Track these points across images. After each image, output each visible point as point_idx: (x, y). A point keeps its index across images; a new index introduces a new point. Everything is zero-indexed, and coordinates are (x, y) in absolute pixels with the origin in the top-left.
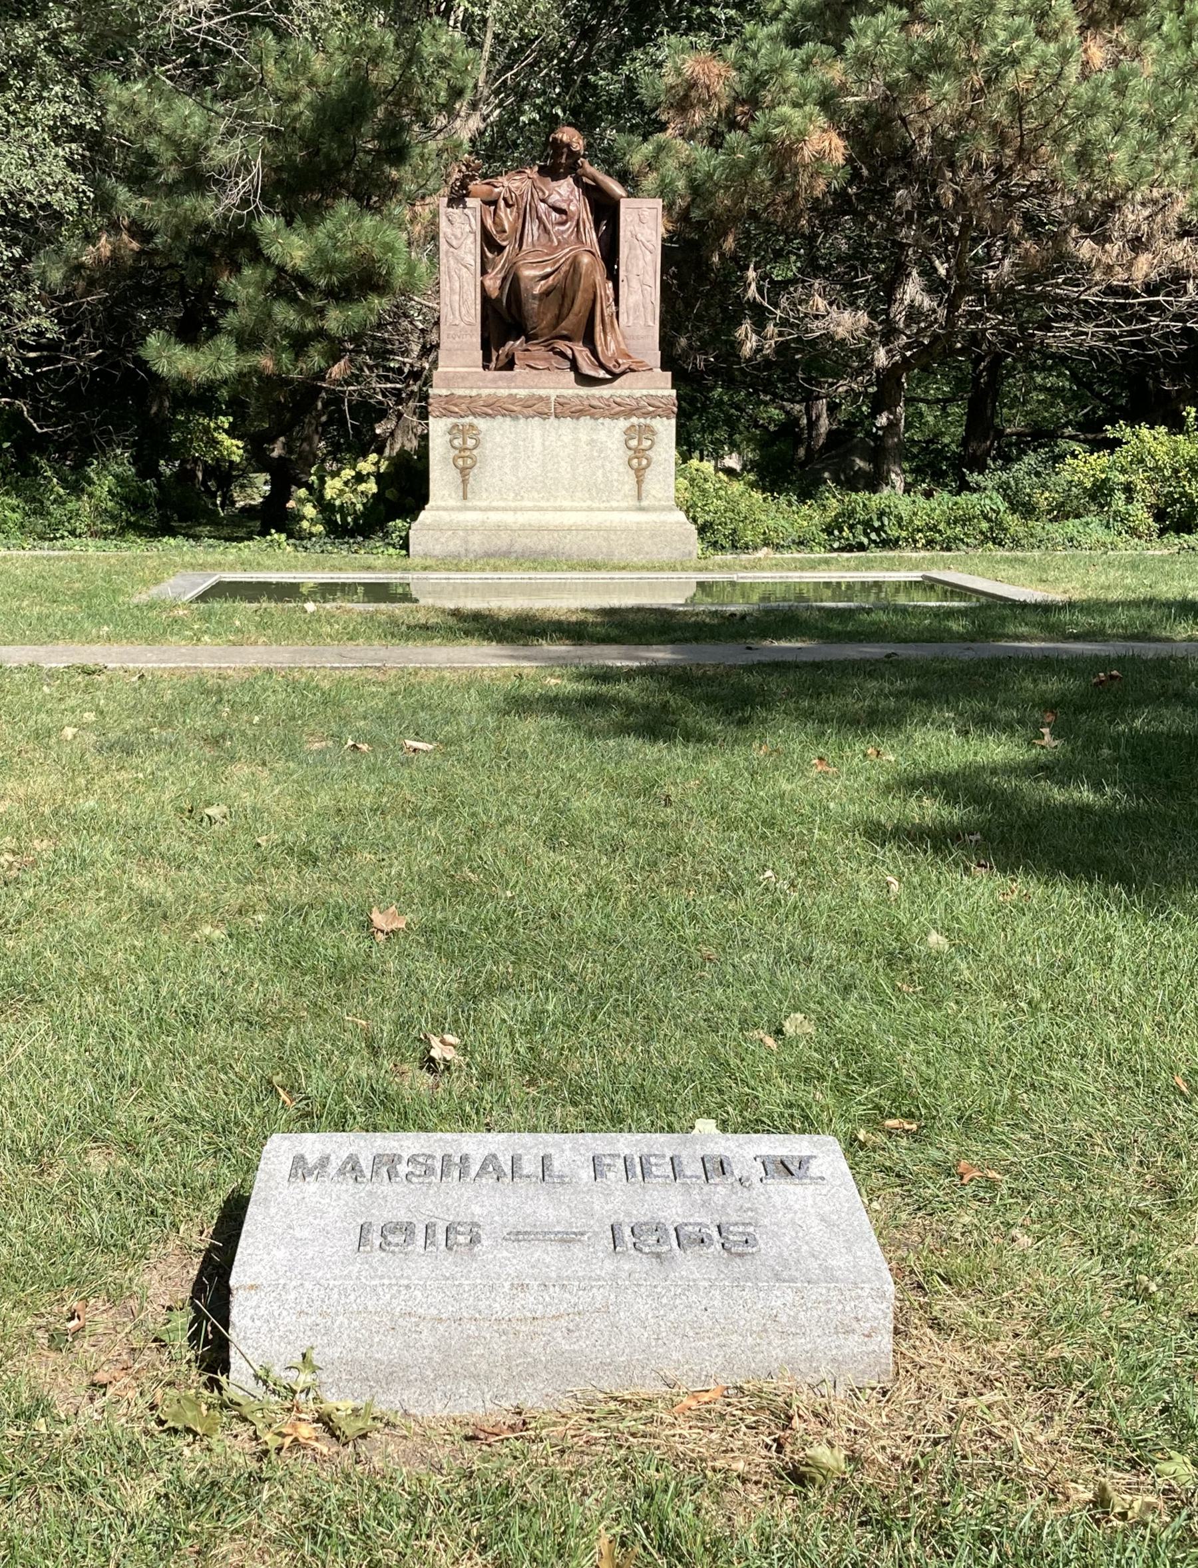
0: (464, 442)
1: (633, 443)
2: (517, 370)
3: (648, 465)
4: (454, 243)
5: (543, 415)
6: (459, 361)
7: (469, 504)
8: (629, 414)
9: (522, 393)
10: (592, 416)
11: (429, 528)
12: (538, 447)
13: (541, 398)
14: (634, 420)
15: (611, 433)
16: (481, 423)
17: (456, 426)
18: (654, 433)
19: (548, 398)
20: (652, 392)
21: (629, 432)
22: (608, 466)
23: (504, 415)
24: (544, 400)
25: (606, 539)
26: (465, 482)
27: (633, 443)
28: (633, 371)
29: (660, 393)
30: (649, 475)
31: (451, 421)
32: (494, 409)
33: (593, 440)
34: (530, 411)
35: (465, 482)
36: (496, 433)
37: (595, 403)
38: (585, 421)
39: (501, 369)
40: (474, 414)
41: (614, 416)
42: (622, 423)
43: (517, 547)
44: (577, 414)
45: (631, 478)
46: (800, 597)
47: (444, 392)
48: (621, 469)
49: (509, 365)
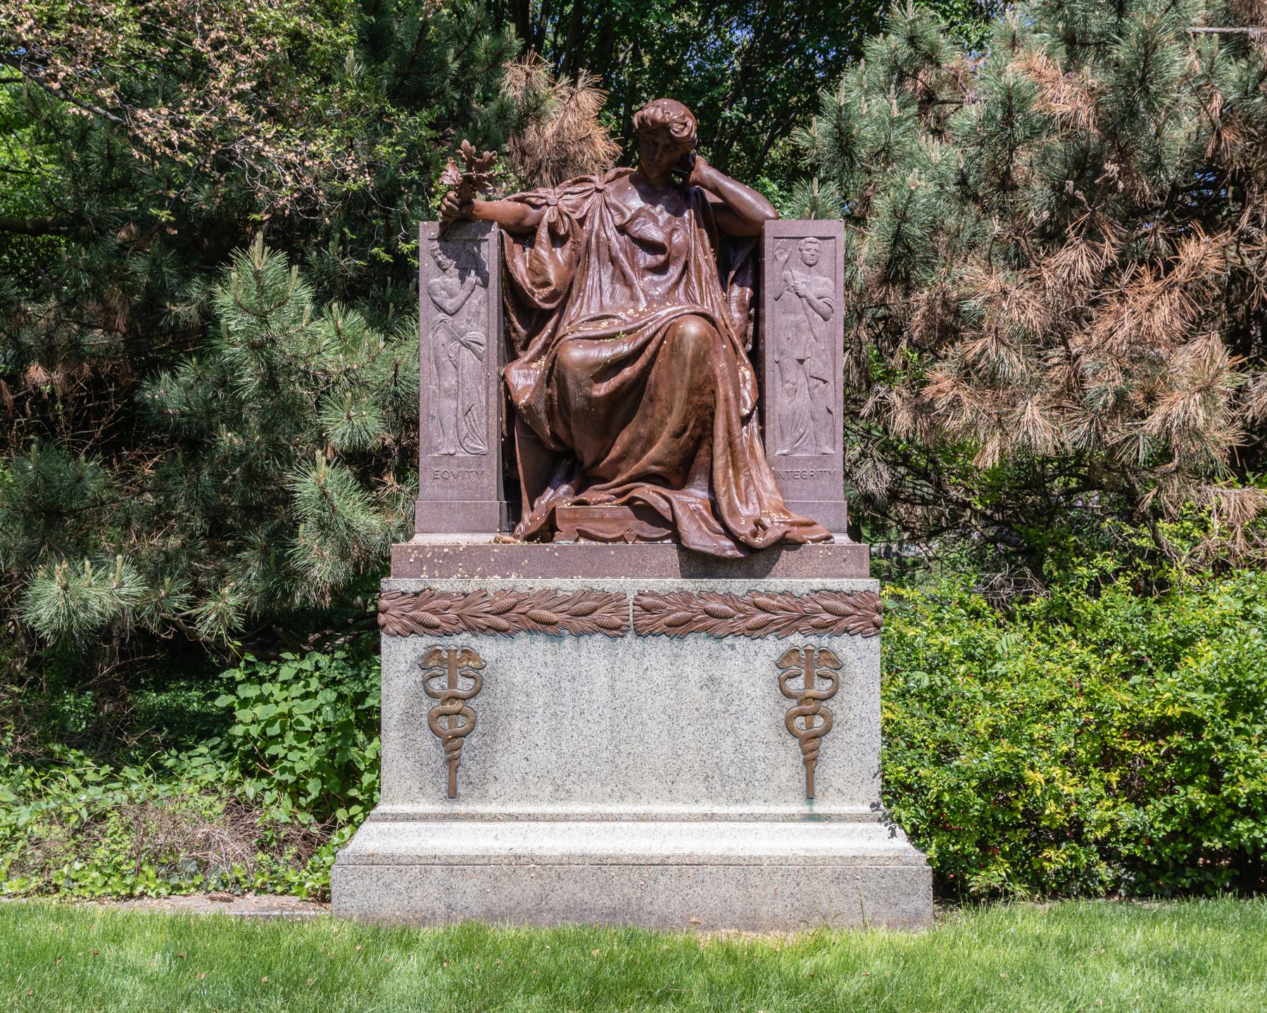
0: (452, 684)
1: (796, 685)
2: (561, 541)
3: (828, 729)
4: (449, 304)
5: (613, 631)
6: (448, 536)
7: (460, 808)
8: (784, 630)
9: (569, 585)
10: (710, 633)
11: (372, 860)
12: (603, 695)
13: (606, 597)
14: (796, 640)
15: (751, 666)
16: (488, 648)
17: (433, 652)
18: (838, 665)
19: (621, 597)
20: (832, 584)
21: (785, 661)
22: (745, 730)
23: (530, 631)
24: (615, 601)
25: (742, 885)
26: (453, 763)
27: (796, 685)
28: (795, 545)
29: (846, 584)
30: (829, 747)
31: (421, 643)
32: (514, 620)
33: (712, 679)
34: (584, 622)
35: (453, 763)
36: (517, 663)
37: (714, 605)
38: (696, 649)
39: (530, 538)
40: (471, 629)
41: (754, 632)
42: (772, 647)
43: (554, 900)
44: (679, 629)
45: (791, 754)
46: (663, 898)
47: (411, 585)
48: (772, 737)
49: (547, 532)
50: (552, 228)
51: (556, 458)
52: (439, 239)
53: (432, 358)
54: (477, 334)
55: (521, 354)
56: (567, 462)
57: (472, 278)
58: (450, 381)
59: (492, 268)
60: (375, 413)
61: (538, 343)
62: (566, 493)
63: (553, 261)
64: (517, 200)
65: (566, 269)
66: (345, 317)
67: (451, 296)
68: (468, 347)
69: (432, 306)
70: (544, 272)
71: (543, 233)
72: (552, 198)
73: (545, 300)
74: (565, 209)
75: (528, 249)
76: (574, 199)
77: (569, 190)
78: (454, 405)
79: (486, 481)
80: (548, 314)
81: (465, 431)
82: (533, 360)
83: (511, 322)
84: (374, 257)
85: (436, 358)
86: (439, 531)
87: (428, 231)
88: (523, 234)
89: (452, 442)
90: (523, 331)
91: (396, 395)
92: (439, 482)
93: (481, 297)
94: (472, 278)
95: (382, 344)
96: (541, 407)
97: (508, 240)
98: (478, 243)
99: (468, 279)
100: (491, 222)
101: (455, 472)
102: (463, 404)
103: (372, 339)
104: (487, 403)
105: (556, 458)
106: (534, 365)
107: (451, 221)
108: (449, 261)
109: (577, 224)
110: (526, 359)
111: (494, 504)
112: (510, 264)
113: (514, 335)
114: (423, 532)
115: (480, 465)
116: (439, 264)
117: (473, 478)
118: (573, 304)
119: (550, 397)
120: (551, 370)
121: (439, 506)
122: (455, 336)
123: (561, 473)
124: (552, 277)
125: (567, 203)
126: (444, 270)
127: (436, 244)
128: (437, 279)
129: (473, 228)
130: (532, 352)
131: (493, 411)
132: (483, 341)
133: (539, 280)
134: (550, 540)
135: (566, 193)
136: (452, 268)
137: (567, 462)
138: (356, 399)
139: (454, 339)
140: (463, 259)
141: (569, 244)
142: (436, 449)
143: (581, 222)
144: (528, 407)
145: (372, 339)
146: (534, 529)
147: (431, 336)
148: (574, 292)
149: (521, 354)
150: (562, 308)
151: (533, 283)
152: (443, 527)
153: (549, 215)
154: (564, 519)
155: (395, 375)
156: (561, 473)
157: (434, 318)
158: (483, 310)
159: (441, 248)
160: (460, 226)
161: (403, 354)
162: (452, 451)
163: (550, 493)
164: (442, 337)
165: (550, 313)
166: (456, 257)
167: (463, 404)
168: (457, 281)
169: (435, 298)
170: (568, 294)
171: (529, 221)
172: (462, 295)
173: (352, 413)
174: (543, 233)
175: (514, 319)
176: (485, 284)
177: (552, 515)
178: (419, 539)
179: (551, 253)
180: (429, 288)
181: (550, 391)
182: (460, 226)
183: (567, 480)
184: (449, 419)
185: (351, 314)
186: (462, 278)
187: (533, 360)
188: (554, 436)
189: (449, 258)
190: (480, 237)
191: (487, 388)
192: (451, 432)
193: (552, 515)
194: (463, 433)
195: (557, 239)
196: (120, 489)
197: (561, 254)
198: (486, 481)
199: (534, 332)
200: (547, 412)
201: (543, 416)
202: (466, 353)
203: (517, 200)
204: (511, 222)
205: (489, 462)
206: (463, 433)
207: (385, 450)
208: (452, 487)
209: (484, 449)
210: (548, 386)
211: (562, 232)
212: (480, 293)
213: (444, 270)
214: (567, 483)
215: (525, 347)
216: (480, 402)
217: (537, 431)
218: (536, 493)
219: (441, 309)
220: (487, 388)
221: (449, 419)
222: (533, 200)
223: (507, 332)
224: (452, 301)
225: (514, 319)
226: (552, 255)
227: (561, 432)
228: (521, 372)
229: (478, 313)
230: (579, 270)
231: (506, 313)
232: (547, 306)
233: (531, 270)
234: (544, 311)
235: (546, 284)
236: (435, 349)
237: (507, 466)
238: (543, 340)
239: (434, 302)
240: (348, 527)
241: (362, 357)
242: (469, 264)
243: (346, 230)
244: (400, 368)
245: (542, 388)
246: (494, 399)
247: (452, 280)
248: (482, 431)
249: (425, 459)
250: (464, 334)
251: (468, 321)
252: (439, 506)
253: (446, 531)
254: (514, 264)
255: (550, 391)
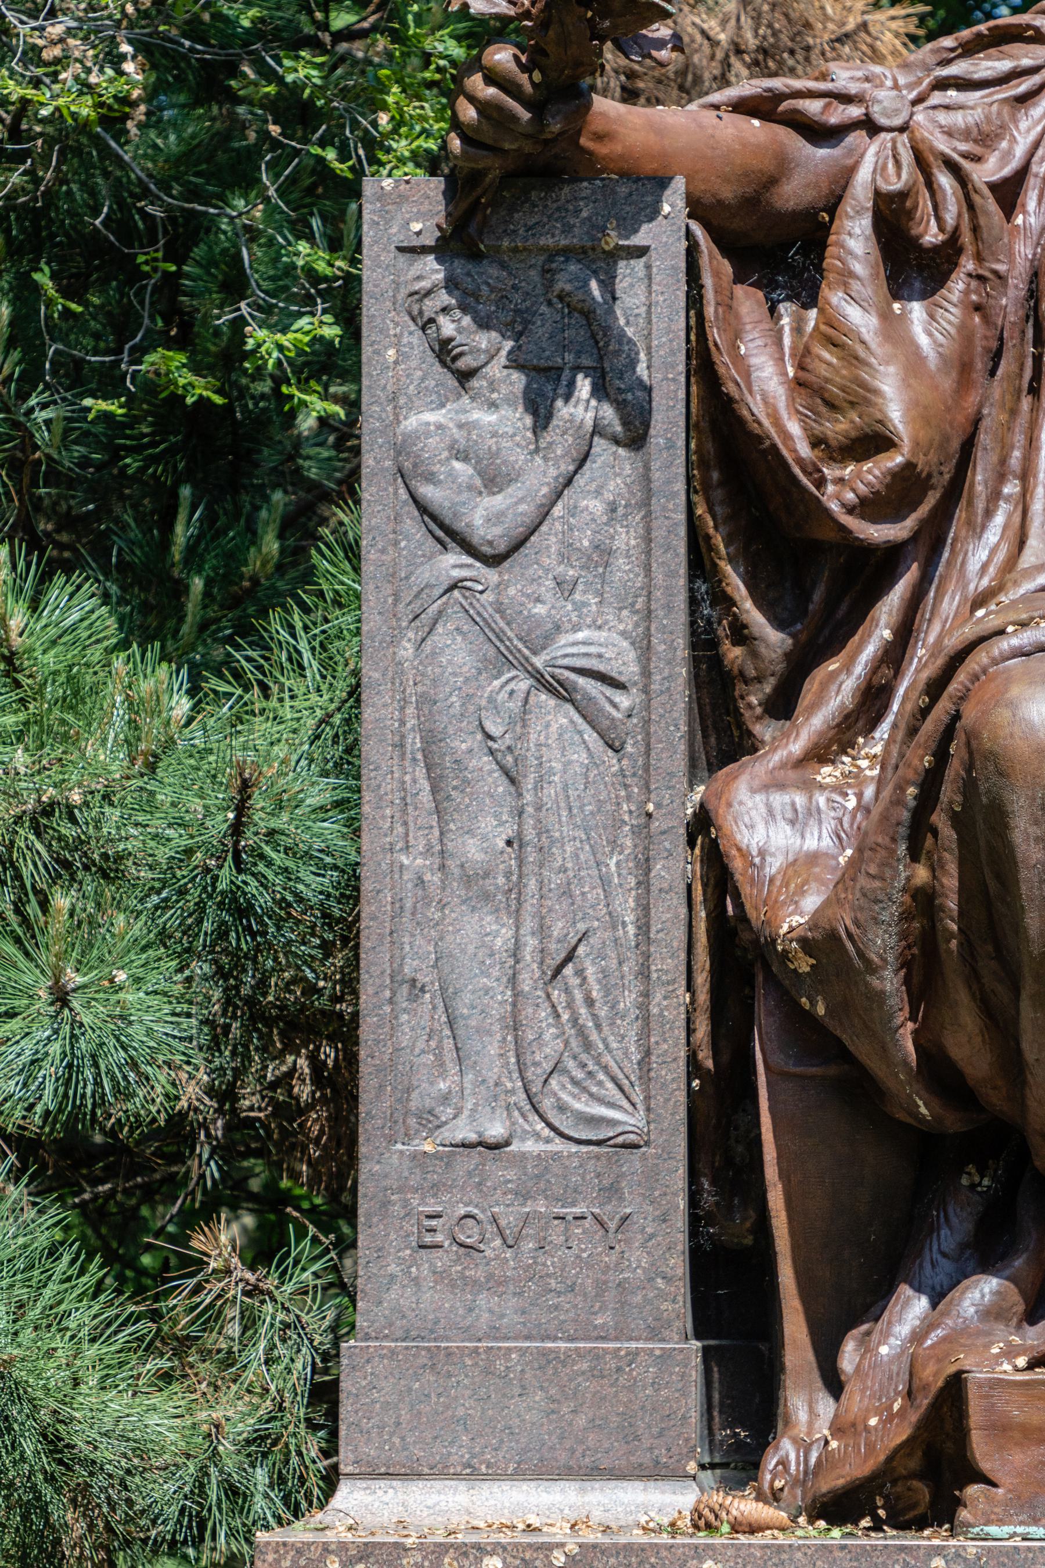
4: (485, 516)
39: (838, 1508)
50: (891, 217)
51: (927, 1162)
52: (442, 249)
53: (414, 742)
54: (599, 638)
55: (765, 730)
56: (976, 1181)
57: (582, 407)
58: (483, 836)
59: (661, 367)
60: (154, 980)
61: (838, 685)
62: (993, 1313)
63: (902, 354)
64: (744, 107)
65: (947, 383)
66: (35, 606)
67: (493, 480)
68: (559, 689)
69: (412, 526)
70: (861, 396)
71: (855, 239)
72: (887, 102)
73: (870, 507)
74: (942, 145)
75: (787, 310)
76: (975, 108)
77: (958, 69)
78: (503, 938)
79: (638, 1258)
80: (875, 569)
81: (548, 1045)
82: (820, 754)
83: (724, 600)
84: (150, 387)
85: (431, 740)
86: (440, 1472)
87: (402, 207)
88: (771, 244)
89: (496, 1095)
90: (774, 640)
91: (239, 908)
92: (440, 1260)
93: (615, 486)
94: (582, 407)
95: (182, 705)
96: (883, 942)
97: (716, 267)
98: (604, 262)
99: (564, 411)
100: (662, 182)
101: (509, 1220)
102: (542, 931)
103: (146, 686)
104: (644, 927)
105: (927, 1162)
106: (827, 774)
107: (494, 167)
108: (484, 340)
109: (990, 205)
110: (797, 747)
111: (675, 1366)
112: (723, 361)
113: (734, 654)
114: (373, 1473)
115: (612, 1191)
116: (444, 352)
117: (585, 1242)
118: (977, 530)
119: (924, 902)
120: (930, 783)
121: (439, 1361)
122: (509, 649)
123: (952, 1231)
124: (896, 414)
125: (940, 125)
126: (465, 377)
127: (431, 270)
128: (439, 416)
129: (583, 202)
130: (815, 721)
131: (668, 962)
132: (625, 663)
133: (839, 427)
134: (942, 1512)
135: (942, 85)
136: (496, 369)
137: (976, 1181)
138: (85, 925)
139: (506, 659)
140: (541, 330)
141: (957, 286)
142: (429, 1121)
143: (1009, 192)
144: (823, 943)
145: (146, 686)
146: (856, 1468)
147: (406, 650)
148: (980, 478)
149: (765, 730)
150: (932, 541)
151: (816, 442)
152: (459, 1454)
153: (874, 167)
154: (1002, 1430)
155: (237, 829)
156: (952, 1231)
157: (424, 574)
158: (625, 538)
159: (451, 284)
160: (525, 197)
161: (278, 739)
162: (496, 1131)
163: (911, 1309)
164: (456, 651)
165: (885, 563)
166: (517, 326)
167: (542, 931)
168: (514, 419)
169: (427, 491)
170: (956, 488)
171: (794, 193)
172: (539, 477)
173: (73, 978)
174: (855, 239)
175: (736, 585)
176: (635, 436)
177: (946, 1409)
178: (361, 1506)
179: (886, 316)
180: (400, 449)
181: (922, 874)
182: (525, 197)
183: (984, 1254)
184: (483, 994)
185: (57, 592)
186: (539, 410)
187: (820, 754)
188: (936, 1068)
189: (483, 324)
190: (613, 239)
191: (645, 866)
192: (491, 1052)
193: (946, 1409)
194: (545, 1054)
195: (911, 266)
196: (272, 1325)
197: (928, 326)
198: (638, 1258)
199: (820, 641)
200: (906, 964)
201: (889, 982)
202: (556, 718)
203: (744, 107)
204: (728, 193)
205: (652, 1176)
206: (545, 1054)
207: (178, 1131)
208: (495, 1284)
209: (629, 1120)
210: (914, 855)
211: (932, 236)
212: (612, 470)
213: (465, 377)
214: (986, 1265)
215: (783, 706)
216: (614, 922)
217: (861, 1049)
218: (849, 1305)
219: (450, 534)
220: (645, 866)
221: (483, 994)
222: (813, 107)
223: (703, 648)
224: (498, 501)
225: (736, 585)
226: (893, 328)
227: (967, 1046)
228: (779, 800)
229: (603, 553)
230: (997, 389)
231: (699, 562)
232: (879, 533)
233: (802, 384)
234: (865, 550)
235: (874, 442)
236: (426, 701)
237: (709, 1199)
238: (860, 668)
239: (423, 508)
240: (54, 1444)
241: (104, 754)
242: (566, 349)
243: (43, 278)
244: (258, 801)
245: (889, 861)
246: (670, 914)
247: (497, 416)
248: (621, 1046)
249: (383, 1163)
250: (548, 639)
251: (565, 587)
252: (439, 1361)
253: (471, 1473)
254: (739, 360)
255: (922, 874)
